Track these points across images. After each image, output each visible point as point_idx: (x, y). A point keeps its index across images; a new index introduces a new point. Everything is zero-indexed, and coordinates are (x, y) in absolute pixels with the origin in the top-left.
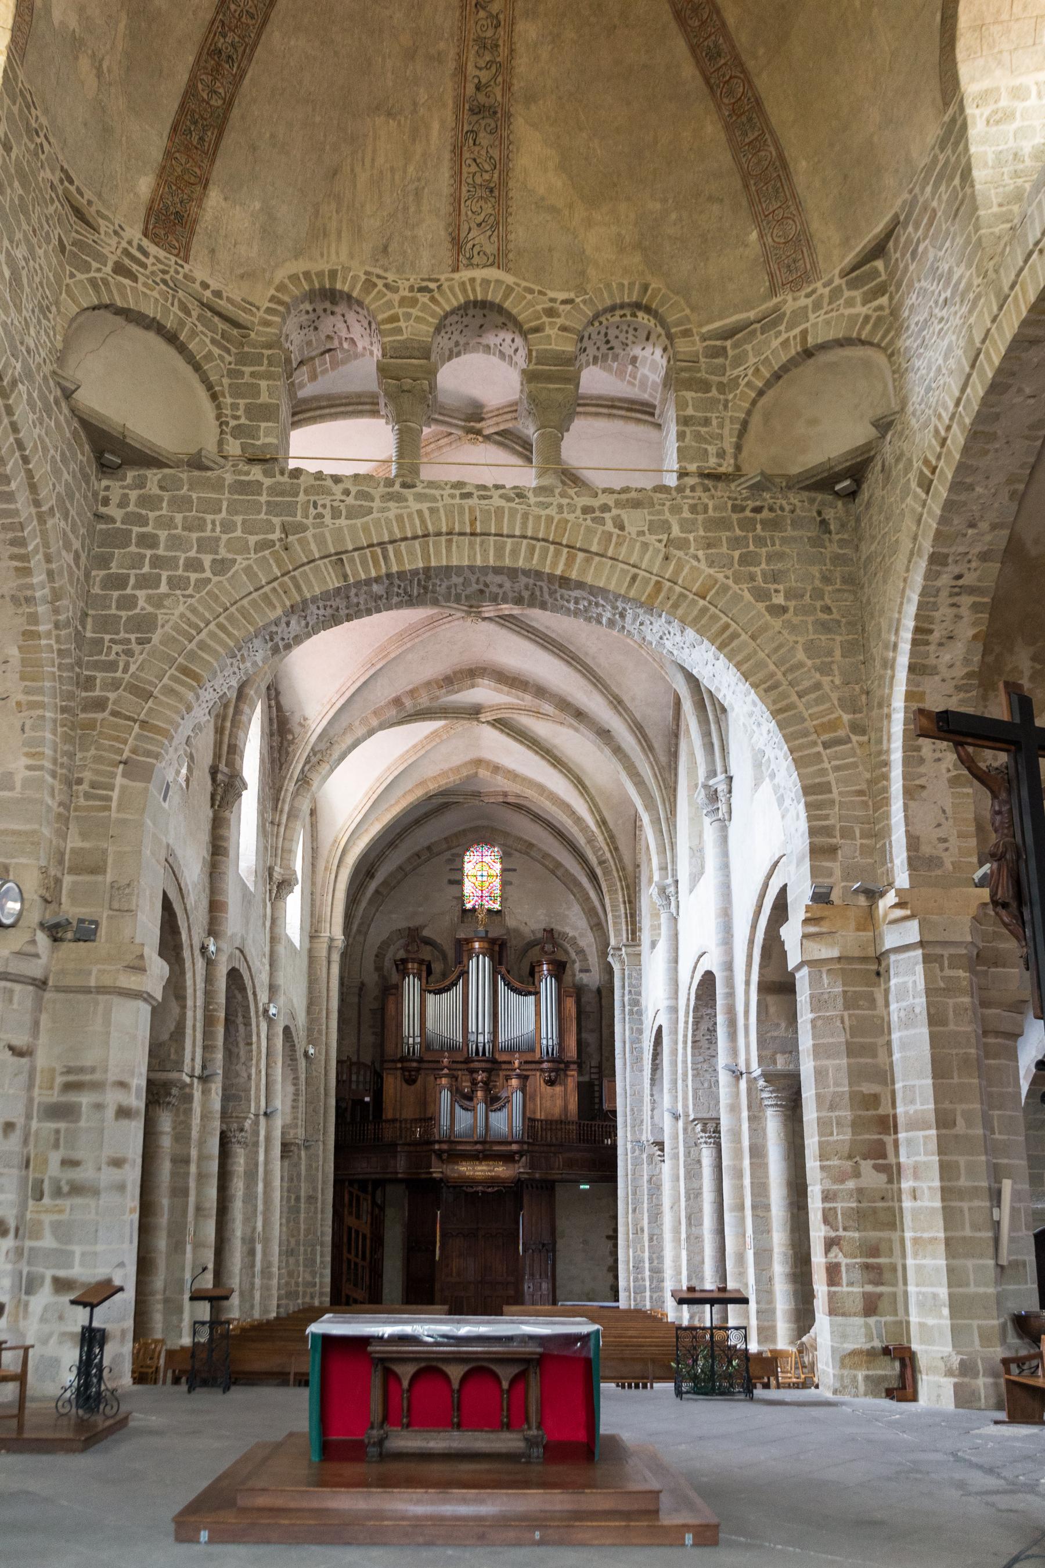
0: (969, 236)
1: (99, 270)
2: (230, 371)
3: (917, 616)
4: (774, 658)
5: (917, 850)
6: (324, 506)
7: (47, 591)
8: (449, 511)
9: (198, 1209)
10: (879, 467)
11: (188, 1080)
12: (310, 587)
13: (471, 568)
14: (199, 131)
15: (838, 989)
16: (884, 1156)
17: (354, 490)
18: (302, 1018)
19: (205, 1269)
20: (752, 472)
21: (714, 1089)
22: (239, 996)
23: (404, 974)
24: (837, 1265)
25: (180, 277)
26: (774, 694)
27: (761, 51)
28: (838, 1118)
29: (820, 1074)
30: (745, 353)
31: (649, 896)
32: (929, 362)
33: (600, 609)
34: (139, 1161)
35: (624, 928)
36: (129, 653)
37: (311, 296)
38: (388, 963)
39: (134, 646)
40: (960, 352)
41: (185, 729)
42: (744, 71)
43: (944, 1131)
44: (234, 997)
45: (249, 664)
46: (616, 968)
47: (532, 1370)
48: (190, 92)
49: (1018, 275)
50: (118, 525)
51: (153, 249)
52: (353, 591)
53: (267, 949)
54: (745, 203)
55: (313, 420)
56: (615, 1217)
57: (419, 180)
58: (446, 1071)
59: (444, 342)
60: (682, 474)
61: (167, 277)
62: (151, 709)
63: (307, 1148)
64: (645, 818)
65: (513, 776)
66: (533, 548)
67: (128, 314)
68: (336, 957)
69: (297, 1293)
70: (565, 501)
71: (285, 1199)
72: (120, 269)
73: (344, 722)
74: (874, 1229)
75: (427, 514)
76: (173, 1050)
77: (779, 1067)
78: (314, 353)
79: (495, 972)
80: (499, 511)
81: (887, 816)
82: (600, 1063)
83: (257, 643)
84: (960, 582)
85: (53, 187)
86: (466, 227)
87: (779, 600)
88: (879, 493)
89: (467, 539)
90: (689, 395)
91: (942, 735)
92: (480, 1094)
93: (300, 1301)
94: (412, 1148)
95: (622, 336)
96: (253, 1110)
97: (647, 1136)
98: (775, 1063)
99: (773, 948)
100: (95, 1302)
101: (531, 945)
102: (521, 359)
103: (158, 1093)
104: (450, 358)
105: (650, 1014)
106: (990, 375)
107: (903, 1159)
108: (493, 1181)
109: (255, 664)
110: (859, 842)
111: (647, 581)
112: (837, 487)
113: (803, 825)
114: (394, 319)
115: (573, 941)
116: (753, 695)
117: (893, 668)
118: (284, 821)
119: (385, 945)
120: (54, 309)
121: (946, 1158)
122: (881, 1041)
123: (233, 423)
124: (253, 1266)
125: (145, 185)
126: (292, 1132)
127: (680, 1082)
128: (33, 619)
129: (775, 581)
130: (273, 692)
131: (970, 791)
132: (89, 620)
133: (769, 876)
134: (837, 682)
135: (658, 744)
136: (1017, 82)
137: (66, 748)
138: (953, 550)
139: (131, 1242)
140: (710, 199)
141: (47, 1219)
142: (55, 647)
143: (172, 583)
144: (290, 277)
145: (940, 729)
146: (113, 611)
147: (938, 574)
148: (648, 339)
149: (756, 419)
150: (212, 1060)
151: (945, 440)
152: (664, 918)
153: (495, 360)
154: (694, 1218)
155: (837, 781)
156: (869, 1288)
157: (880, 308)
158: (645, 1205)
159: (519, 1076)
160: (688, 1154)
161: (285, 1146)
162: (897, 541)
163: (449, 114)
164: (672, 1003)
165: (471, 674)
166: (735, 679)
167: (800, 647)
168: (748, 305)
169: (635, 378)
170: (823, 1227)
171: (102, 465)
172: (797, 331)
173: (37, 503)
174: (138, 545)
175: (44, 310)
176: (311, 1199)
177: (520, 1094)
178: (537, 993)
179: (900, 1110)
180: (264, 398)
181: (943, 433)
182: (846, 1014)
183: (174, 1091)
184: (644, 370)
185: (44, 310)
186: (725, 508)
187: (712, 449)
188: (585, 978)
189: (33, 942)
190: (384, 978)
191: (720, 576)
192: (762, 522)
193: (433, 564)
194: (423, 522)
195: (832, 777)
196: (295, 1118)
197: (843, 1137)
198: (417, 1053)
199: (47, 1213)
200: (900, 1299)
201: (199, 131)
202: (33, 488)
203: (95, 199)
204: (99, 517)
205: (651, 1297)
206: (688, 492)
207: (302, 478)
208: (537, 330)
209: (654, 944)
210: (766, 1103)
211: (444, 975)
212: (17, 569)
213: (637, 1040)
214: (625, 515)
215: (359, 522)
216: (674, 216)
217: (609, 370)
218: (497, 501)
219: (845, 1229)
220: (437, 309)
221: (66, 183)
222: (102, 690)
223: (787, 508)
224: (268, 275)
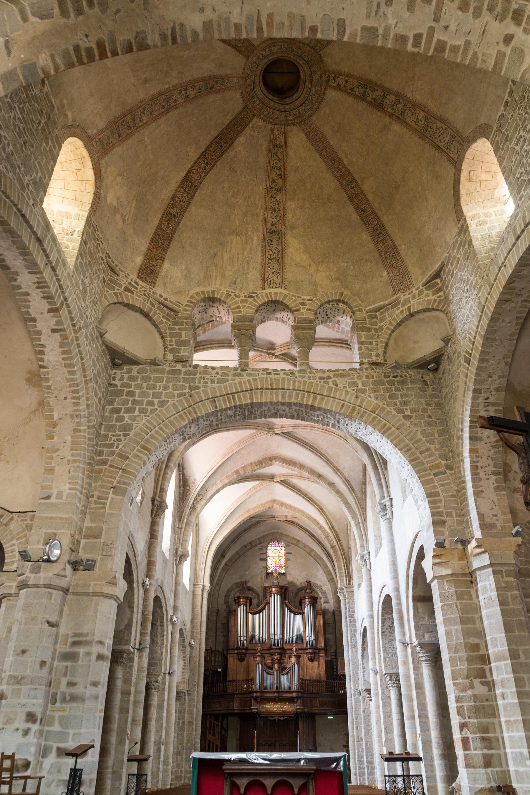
0: (474, 265)
1: (118, 290)
2: (170, 328)
3: (470, 416)
4: (408, 437)
5: (483, 521)
6: (208, 379)
7: (86, 412)
8: (262, 380)
9: (133, 720)
10: (446, 357)
11: (132, 650)
12: (201, 411)
13: (271, 402)
14: (161, 242)
15: (453, 590)
16: (485, 677)
17: (220, 372)
18: (188, 626)
19: (136, 743)
20: (391, 362)
21: (394, 657)
22: (159, 611)
23: (239, 604)
24: (467, 738)
25: (151, 293)
26: (409, 452)
27: (383, 209)
29: (448, 634)
30: (385, 316)
31: (356, 562)
32: (464, 314)
33: (328, 420)
34: (106, 684)
35: (345, 578)
36: (119, 440)
37: (204, 300)
38: (231, 600)
39: (122, 437)
40: (476, 308)
41: (142, 474)
42: (376, 216)
43: (514, 661)
44: (157, 611)
45: (172, 445)
46: (342, 598)
47: (310, 781)
48: (159, 227)
49: (497, 276)
50: (119, 388)
51: (141, 283)
52: (219, 413)
53: (173, 588)
54: (380, 262)
55: (203, 349)
56: (347, 735)
58: (259, 654)
59: (259, 316)
60: (362, 363)
61: (146, 293)
62: (127, 464)
63: (189, 694)
64: (352, 523)
65: (290, 507)
66: (298, 394)
67: (129, 306)
68: (206, 595)
69: (181, 776)
70: (311, 375)
71: (177, 723)
72: (126, 289)
73: (213, 481)
74: (485, 717)
75: (252, 381)
76: (125, 634)
77: (426, 640)
79: (283, 603)
80: (283, 380)
81: (467, 506)
82: (336, 650)
83: (176, 435)
84: (488, 401)
85: (102, 259)
87: (408, 413)
88: (447, 367)
89: (269, 391)
90: (362, 333)
91: (492, 427)
92: (276, 666)
93: (182, 782)
94: (241, 696)
95: (333, 313)
96: (163, 671)
97: (361, 686)
98: (424, 638)
99: (419, 574)
100: (79, 753)
101: (301, 589)
102: (291, 322)
103: (118, 657)
104: (261, 323)
105: (360, 621)
106: (490, 315)
107: (495, 678)
108: (283, 714)
109: (175, 445)
110: (455, 519)
111: (349, 406)
112: (429, 367)
113: (428, 512)
114: (238, 307)
115: (320, 588)
116: (400, 454)
117: (462, 439)
118: (184, 527)
119: (229, 591)
120: (99, 303)
121: (517, 675)
122: (477, 616)
123: (170, 347)
124: (159, 758)
125: (139, 260)
126: (182, 686)
127: (377, 654)
128: (79, 424)
129: (405, 405)
130: (181, 468)
131: (505, 493)
132: (103, 426)
133: (414, 543)
134: (438, 447)
135: (357, 488)
136: (487, 211)
137: (88, 481)
138: (483, 387)
139: (99, 729)
140: (366, 261)
141: (57, 714)
142: (87, 437)
143: (140, 411)
144: (196, 293)
145: (490, 425)
146: (114, 423)
147: (478, 398)
149: (392, 341)
150: (145, 640)
151: (474, 342)
152: (364, 571)
153: (280, 324)
154: (388, 729)
155: (442, 491)
156: (486, 751)
157: (440, 296)
158: (363, 725)
159: (296, 656)
160: (383, 693)
161: (177, 693)
162: (458, 386)
163: (260, 234)
164: (370, 613)
165: (270, 460)
166: (391, 447)
167: (419, 433)
170: (457, 717)
171: (114, 364)
172: (406, 307)
173: (85, 376)
174: (126, 396)
175: (95, 303)
176: (190, 723)
177: (296, 666)
178: (303, 613)
179: (491, 651)
180: (184, 338)
181: (473, 340)
182: (458, 602)
183: (125, 656)
184: (343, 326)
185: (95, 303)
186: (381, 376)
187: (374, 354)
188: (327, 606)
189: (64, 569)
190: (228, 607)
191: (381, 404)
192: (397, 381)
193: (254, 401)
194: (250, 384)
195: (439, 489)
196: (183, 678)
197: (463, 667)
198: (245, 646)
199: (57, 712)
200: (503, 758)
201: (161, 242)
202: (84, 370)
203: (118, 264)
204: (110, 385)
205: (368, 778)
206: (364, 370)
207: (198, 368)
208: (297, 310)
209: (359, 586)
210: (422, 659)
211: (258, 606)
212: (74, 403)
213: (354, 636)
214: (338, 380)
215: (222, 385)
216: (352, 268)
217: (328, 326)
218: (282, 376)
219: (469, 718)
222: (106, 456)
223: (408, 376)
224: (187, 293)
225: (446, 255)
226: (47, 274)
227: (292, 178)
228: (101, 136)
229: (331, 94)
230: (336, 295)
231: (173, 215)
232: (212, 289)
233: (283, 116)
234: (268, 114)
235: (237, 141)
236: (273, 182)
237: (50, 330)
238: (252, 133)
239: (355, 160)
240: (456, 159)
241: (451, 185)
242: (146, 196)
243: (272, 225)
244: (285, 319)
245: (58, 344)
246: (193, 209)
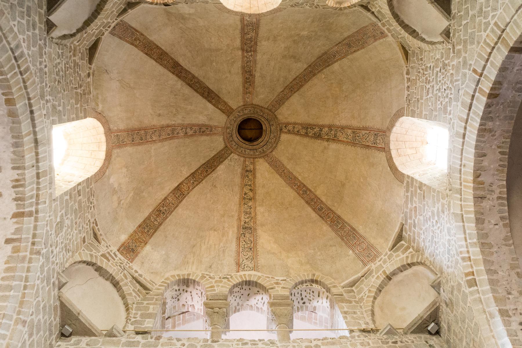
10: (444, 305)
17: (187, 344)
25: (127, 266)
27: (336, 204)
30: (362, 288)
48: (148, 218)
51: (119, 256)
54: (344, 244)
57: (224, 247)
61: (122, 265)
78: (175, 314)
86: (242, 260)
90: (343, 304)
95: (308, 295)
123: (133, 320)
125: (124, 238)
140: (331, 246)
148: (319, 296)
149: (377, 310)
153: (254, 313)
162: (476, 324)
168: (357, 272)
169: (316, 320)
172: (381, 272)
184: (320, 313)
201: (148, 228)
206: (357, 338)
216: (319, 253)
220: (230, 283)
221: (95, 225)
224: (162, 274)
225: (402, 215)
226: (30, 174)
227: (260, 192)
228: (119, 134)
229: (284, 137)
230: (308, 276)
231: (162, 212)
232: (187, 273)
233: (252, 153)
234: (242, 151)
235: (218, 168)
236: (245, 194)
237: (4, 240)
238: (230, 163)
239: (307, 176)
241: (386, 164)
242: (143, 192)
243: (245, 223)
244: (260, 305)
245: (5, 259)
246: (180, 210)
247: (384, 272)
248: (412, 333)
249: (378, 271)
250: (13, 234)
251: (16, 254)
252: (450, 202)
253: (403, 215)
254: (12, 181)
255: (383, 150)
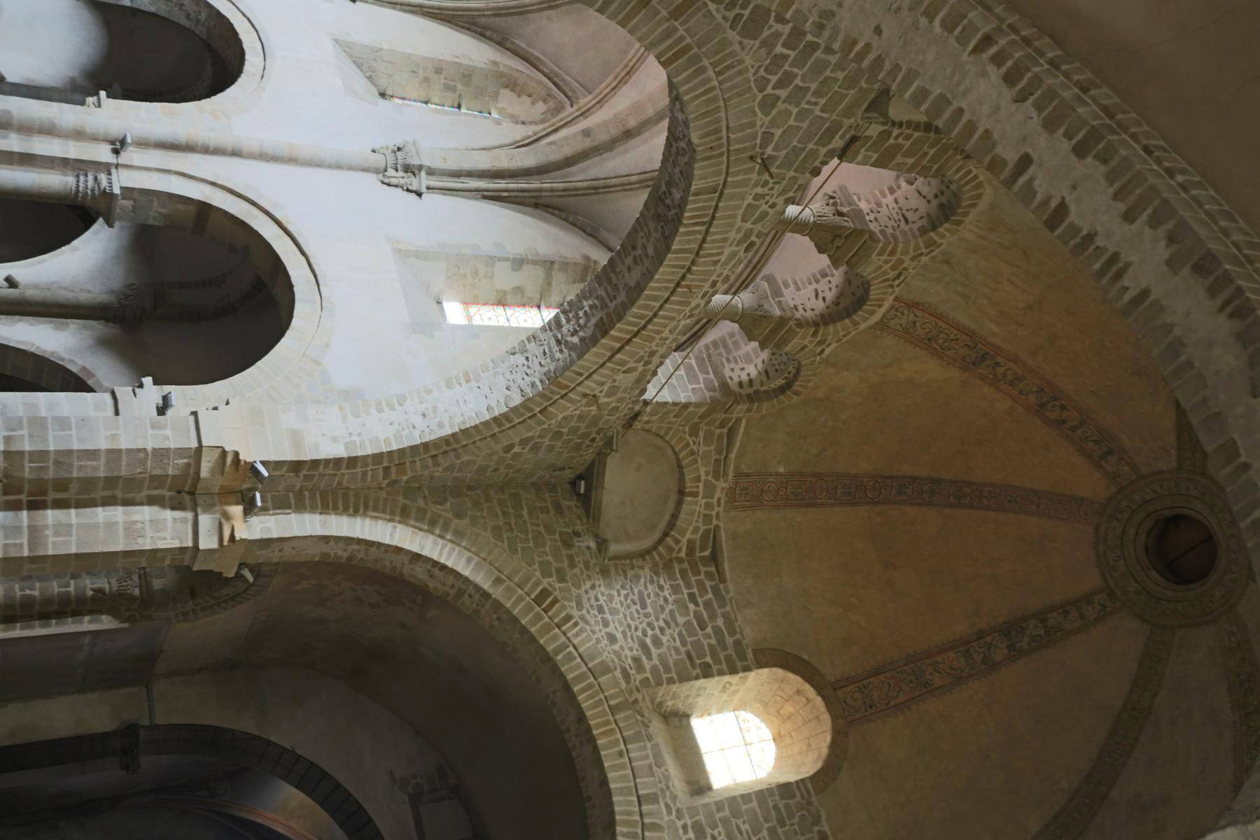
10: (579, 528)
28: (47, 468)
42: (878, 502)
112: (583, 483)
172: (701, 489)
210: (82, 178)
212: (855, 42)
236: (1063, 408)
237: (1035, 156)
240: (840, 693)
245: (996, 135)
247: (695, 495)
248: (593, 462)
249: (705, 486)
250: (1032, 179)
251: (988, 159)
252: (628, 682)
253: (728, 597)
254: (1128, 265)
255: (836, 686)
